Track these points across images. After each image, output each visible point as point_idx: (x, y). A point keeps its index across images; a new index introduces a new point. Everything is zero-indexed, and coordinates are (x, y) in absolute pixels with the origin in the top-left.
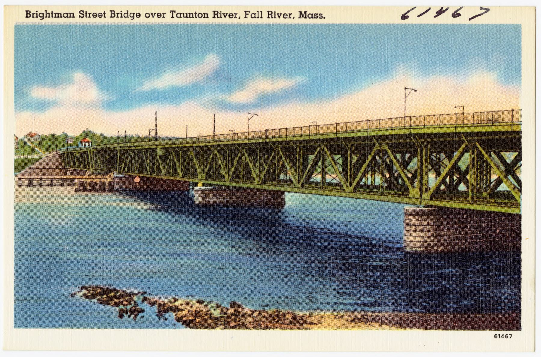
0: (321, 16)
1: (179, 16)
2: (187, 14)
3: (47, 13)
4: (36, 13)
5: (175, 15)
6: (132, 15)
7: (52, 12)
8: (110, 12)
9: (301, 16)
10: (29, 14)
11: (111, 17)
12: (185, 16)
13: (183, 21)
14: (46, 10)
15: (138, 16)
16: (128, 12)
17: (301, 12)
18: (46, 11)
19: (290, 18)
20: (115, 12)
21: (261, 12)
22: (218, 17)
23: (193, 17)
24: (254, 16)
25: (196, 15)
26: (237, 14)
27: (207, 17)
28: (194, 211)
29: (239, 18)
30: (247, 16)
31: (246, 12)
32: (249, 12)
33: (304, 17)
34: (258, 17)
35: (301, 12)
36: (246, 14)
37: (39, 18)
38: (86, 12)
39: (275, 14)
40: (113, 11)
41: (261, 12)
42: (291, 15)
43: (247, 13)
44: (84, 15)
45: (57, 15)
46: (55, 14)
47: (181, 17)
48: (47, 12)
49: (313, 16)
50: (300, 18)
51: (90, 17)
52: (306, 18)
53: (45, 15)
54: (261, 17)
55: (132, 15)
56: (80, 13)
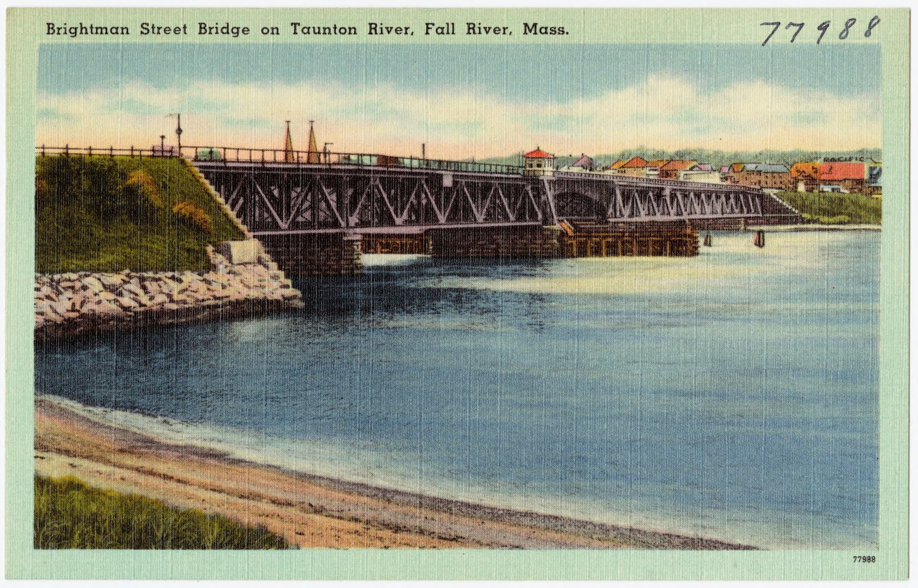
0: (562, 31)
1: (307, 30)
2: (319, 28)
3: (82, 28)
4: (215, 26)
5: (299, 29)
6: (235, 31)
7: (92, 25)
8: (47, 26)
9: (528, 31)
10: (204, 28)
11: (200, 33)
12: (317, 31)
13: (312, 38)
14: (525, 22)
15: (399, 32)
16: (228, 26)
17: (526, 25)
18: (81, 24)
19: (406, 33)
20: (206, 25)
21: (453, 24)
22: (474, 33)
23: (86, 33)
24: (441, 31)
25: (92, 30)
26: (507, 28)
27: (278, 33)
28: (612, 232)
29: (511, 33)
30: (430, 31)
31: (427, 24)
32: (433, 25)
33: (533, 31)
34: (448, 33)
35: (526, 25)
36: (428, 28)
37: (231, 34)
38: (153, 25)
39: (480, 28)
40: (472, 24)
41: (453, 24)
42: (408, 30)
43: (430, 26)
44: (148, 30)
45: (99, 31)
46: (97, 28)
47: (117, 33)
48: (83, 26)
49: (549, 31)
50: (525, 33)
51: (159, 33)
52: (535, 33)
53: (79, 31)
54: (453, 33)
55: (235, 31)
56: (142, 26)
